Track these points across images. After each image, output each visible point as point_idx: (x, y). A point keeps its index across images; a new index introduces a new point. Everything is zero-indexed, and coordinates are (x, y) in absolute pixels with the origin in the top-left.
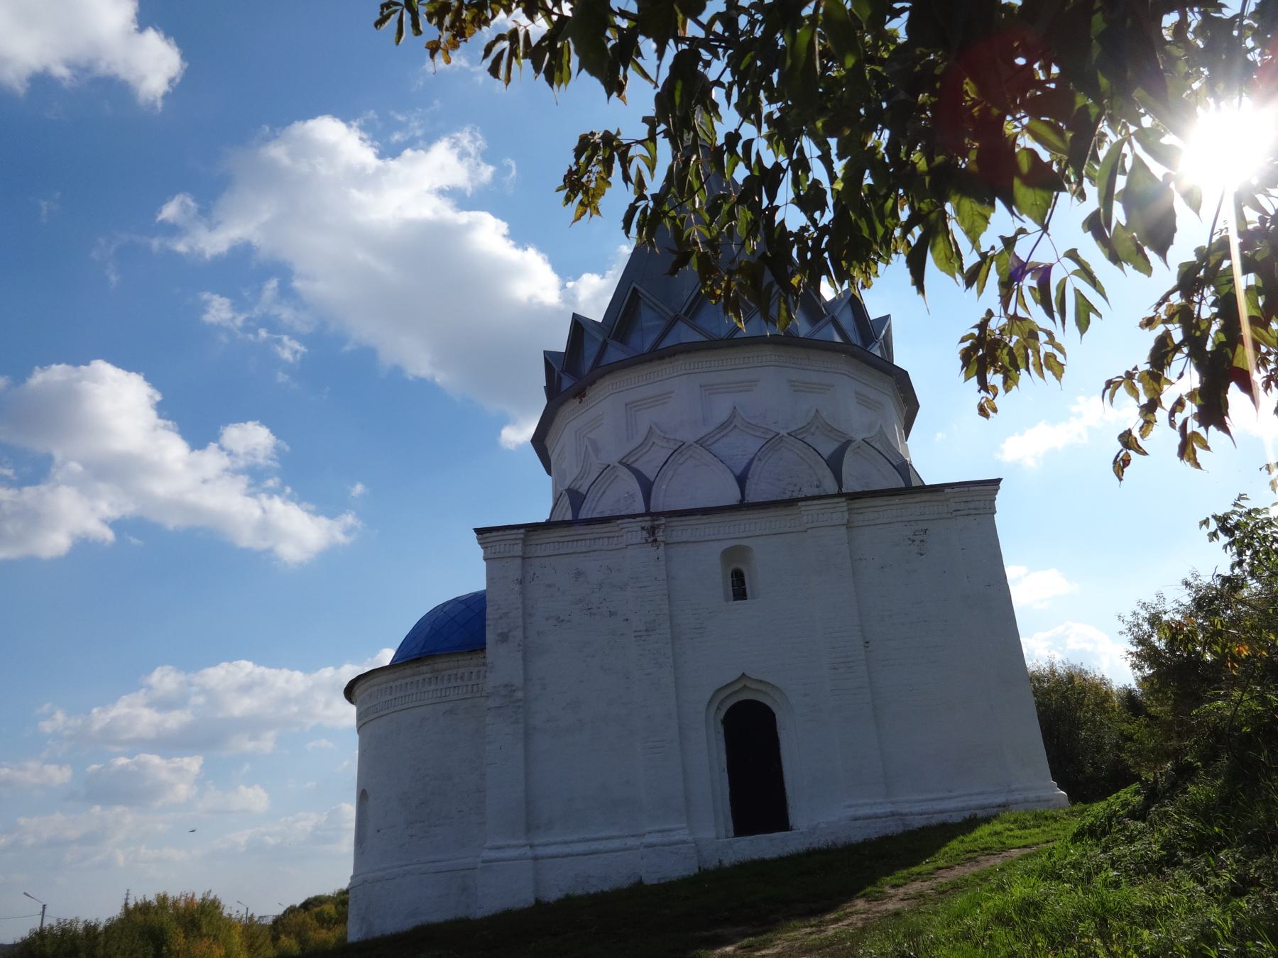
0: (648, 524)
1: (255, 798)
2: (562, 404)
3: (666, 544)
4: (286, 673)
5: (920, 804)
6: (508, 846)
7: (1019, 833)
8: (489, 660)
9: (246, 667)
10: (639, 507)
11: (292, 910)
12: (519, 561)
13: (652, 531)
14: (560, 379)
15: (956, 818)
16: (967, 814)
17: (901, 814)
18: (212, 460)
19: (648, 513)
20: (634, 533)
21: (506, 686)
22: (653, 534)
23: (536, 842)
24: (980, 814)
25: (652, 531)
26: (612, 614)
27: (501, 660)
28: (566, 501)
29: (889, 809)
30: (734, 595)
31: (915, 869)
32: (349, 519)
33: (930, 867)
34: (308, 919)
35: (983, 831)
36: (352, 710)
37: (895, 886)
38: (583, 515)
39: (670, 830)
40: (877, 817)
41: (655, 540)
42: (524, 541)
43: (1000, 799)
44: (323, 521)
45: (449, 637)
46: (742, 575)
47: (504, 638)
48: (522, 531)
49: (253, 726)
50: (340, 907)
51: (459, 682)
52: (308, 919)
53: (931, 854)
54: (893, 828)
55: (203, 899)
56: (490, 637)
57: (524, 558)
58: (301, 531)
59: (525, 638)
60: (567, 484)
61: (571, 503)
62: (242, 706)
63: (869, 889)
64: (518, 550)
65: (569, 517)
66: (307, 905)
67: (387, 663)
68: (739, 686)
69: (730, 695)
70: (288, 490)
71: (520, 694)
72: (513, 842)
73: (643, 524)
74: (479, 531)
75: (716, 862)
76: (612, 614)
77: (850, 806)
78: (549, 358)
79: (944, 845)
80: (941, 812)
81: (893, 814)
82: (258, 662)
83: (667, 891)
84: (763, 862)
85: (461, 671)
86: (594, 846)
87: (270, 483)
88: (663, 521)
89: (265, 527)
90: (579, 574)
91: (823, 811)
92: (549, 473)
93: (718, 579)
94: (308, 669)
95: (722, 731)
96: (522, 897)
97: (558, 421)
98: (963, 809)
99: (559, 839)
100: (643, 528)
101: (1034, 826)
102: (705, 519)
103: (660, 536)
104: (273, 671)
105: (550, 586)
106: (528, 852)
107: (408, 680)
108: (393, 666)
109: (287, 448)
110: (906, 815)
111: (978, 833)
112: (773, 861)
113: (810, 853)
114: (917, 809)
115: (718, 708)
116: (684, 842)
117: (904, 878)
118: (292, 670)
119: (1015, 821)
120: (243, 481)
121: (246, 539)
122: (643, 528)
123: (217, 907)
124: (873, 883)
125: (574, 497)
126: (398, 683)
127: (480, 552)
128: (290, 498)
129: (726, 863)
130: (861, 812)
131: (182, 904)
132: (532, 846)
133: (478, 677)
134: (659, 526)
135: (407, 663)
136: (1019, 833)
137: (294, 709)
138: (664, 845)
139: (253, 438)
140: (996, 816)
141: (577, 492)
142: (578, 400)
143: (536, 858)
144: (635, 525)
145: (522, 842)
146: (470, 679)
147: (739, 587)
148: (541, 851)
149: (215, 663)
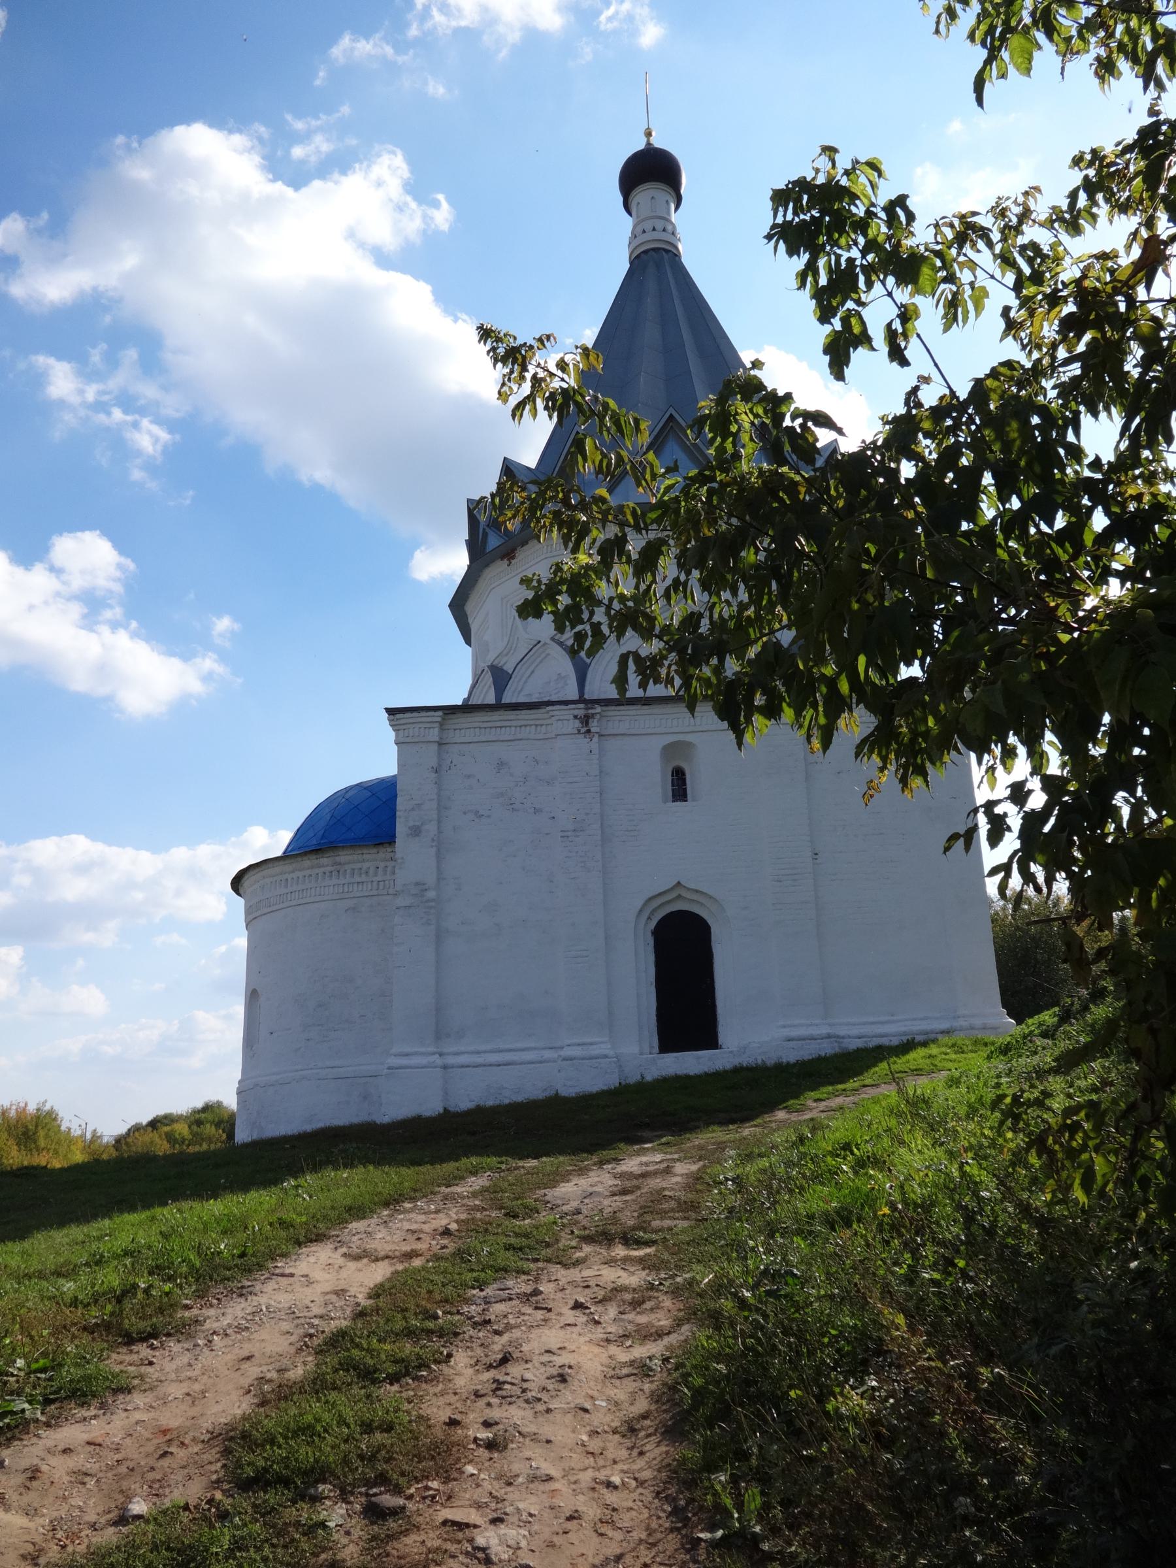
0: (581, 713)
1: (90, 999)
2: (487, 565)
3: (601, 736)
4: (130, 852)
5: (856, 1028)
6: (416, 1054)
7: (953, 1056)
8: (398, 855)
9: (80, 845)
10: (572, 693)
11: (137, 1128)
12: (435, 747)
13: (586, 720)
14: (485, 535)
15: (895, 1042)
16: (905, 1039)
17: (838, 1037)
18: (39, 579)
19: (582, 700)
20: (565, 721)
21: (417, 884)
22: (587, 724)
23: (445, 1051)
24: (919, 1038)
25: (586, 720)
26: (537, 811)
27: (412, 855)
28: (488, 679)
29: (824, 1030)
30: (674, 796)
31: (840, 1087)
32: (209, 663)
33: (856, 1085)
34: (157, 1140)
35: (916, 1057)
36: (240, 902)
37: (816, 1100)
38: (508, 698)
39: (591, 1044)
40: (813, 1038)
41: (589, 731)
42: (441, 725)
43: (945, 1026)
44: (175, 663)
45: (353, 826)
46: (683, 774)
47: (416, 831)
48: (440, 713)
49: (89, 913)
50: (195, 1128)
51: (364, 878)
52: (157, 1140)
53: (861, 1073)
54: (828, 1049)
55: (38, 1110)
56: (401, 829)
57: (440, 744)
58: (149, 677)
59: (440, 832)
60: (491, 658)
61: (495, 682)
62: (73, 890)
63: (791, 1102)
64: (434, 734)
65: (491, 699)
66: (154, 1124)
67: (279, 853)
68: (673, 895)
69: (662, 905)
70: (134, 624)
71: (431, 894)
72: (423, 1050)
73: (576, 712)
74: (391, 712)
75: (639, 1077)
76: (537, 811)
77: (784, 1027)
78: (474, 508)
79: (875, 1065)
80: (881, 1036)
81: (829, 1036)
82: (93, 836)
83: (586, 1101)
84: (687, 1077)
85: (365, 865)
86: (508, 1057)
87: (108, 614)
88: (598, 709)
89: (103, 669)
90: (501, 765)
91: (753, 1026)
92: (468, 641)
93: (657, 779)
94: (155, 849)
95: (652, 943)
96: (431, 1107)
97: (482, 585)
98: (905, 1034)
99: (471, 1048)
100: (575, 717)
101: (972, 1051)
102: (646, 710)
103: (594, 726)
104: (115, 849)
105: (469, 777)
106: (439, 1061)
107: (307, 872)
108: (287, 856)
109: (132, 566)
110: (843, 1038)
111: (912, 1055)
112: (698, 1077)
113: (738, 1070)
114: (855, 1031)
115: (649, 918)
116: (606, 1056)
117: (828, 1093)
118: (137, 848)
119: (953, 1046)
120: (76, 610)
121: (80, 683)
122: (575, 717)
123: (55, 1119)
124: (797, 1097)
125: (500, 677)
126: (295, 875)
127: (391, 734)
128: (134, 635)
129: (649, 1078)
130: (795, 1033)
131: (13, 1113)
132: (441, 1055)
133: (385, 874)
134: (593, 714)
135: (306, 853)
136: (953, 1056)
137: (139, 896)
138: (583, 1059)
139: (90, 555)
140: (934, 1041)
141: (502, 670)
142: (506, 562)
143: (445, 1067)
144: (567, 713)
145: (431, 1049)
146: (376, 874)
147: (679, 787)
148: (450, 1060)
149: (44, 834)
